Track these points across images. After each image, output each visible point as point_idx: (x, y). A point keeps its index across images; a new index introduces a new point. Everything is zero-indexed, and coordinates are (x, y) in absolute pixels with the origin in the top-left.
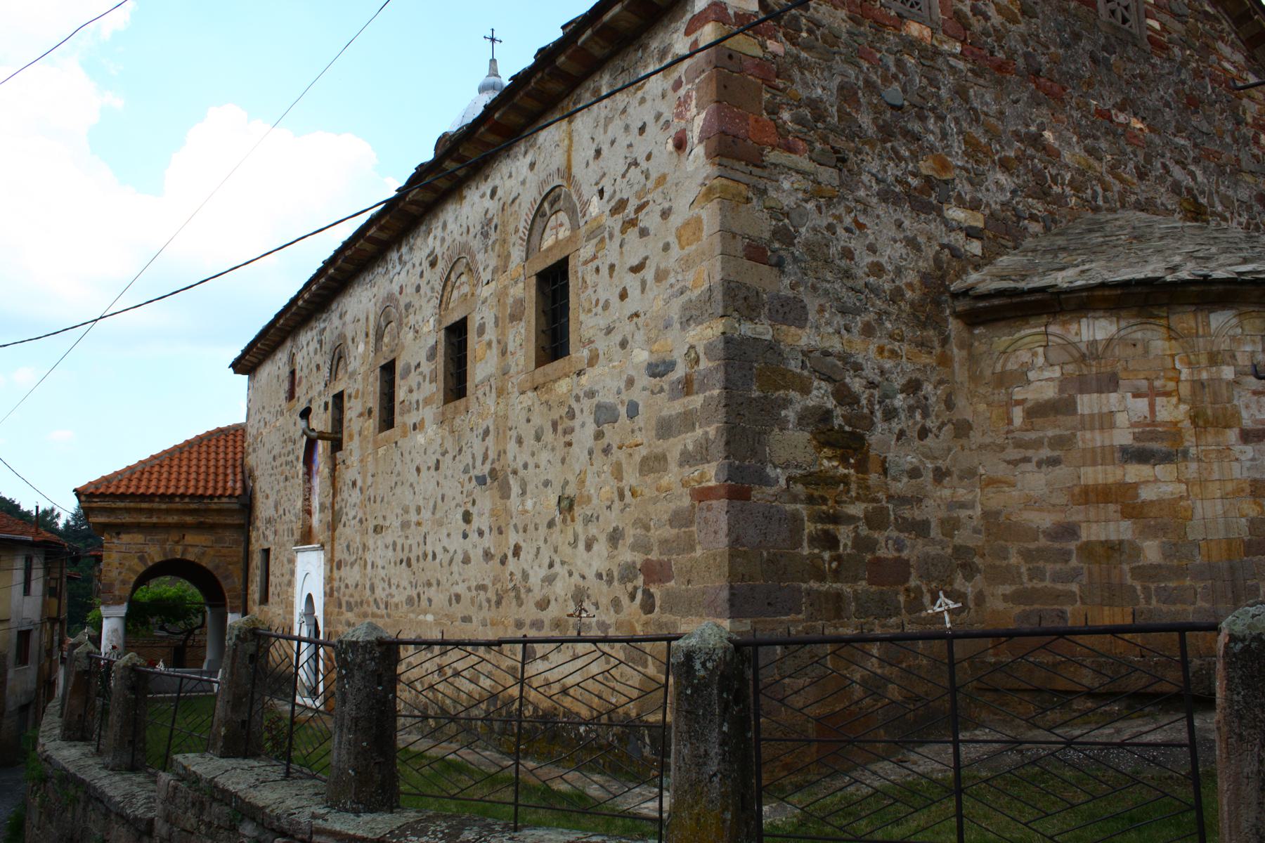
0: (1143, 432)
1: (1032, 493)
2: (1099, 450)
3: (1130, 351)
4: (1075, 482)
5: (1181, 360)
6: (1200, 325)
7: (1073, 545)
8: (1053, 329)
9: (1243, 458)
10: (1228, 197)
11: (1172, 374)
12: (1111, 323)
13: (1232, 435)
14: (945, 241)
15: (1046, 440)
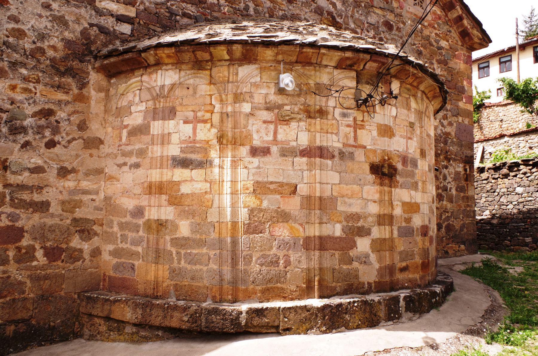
0: (187, 147)
1: (126, 186)
2: (159, 159)
3: (185, 92)
4: (145, 180)
5: (216, 98)
6: (231, 75)
7: (141, 222)
8: (145, 78)
9: (250, 166)
10: (361, 20)
11: (209, 108)
12: (175, 73)
13: (244, 151)
14: (95, 21)
15: (135, 151)
